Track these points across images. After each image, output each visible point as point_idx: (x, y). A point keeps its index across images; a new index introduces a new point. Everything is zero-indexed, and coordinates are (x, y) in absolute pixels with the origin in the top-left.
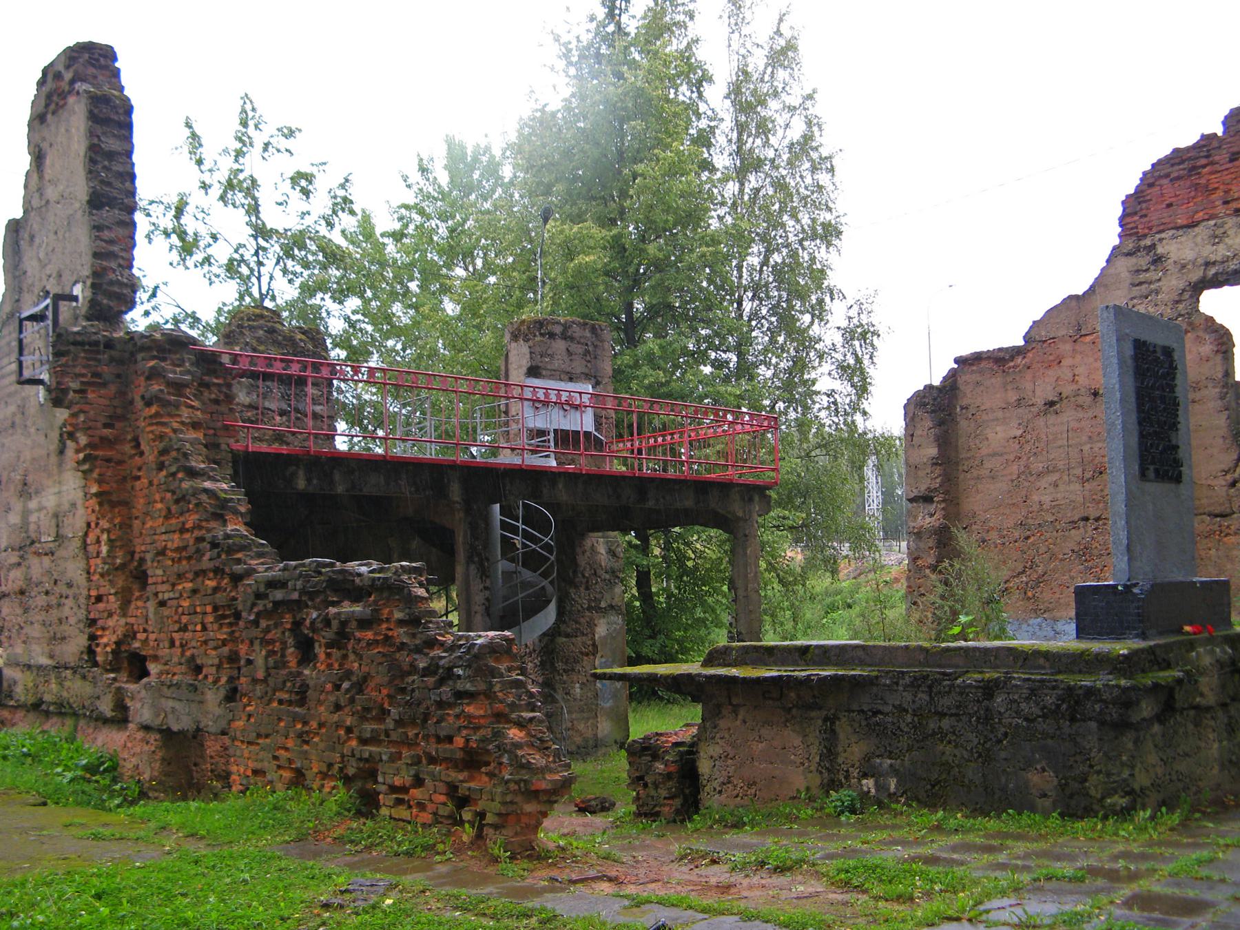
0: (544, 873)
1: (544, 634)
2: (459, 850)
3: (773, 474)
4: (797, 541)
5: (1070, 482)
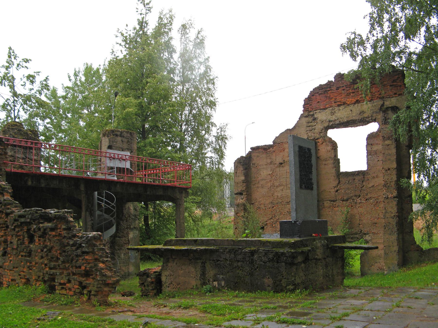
0: (110, 310)
1: (111, 237)
2: (83, 303)
3: (190, 184)
4: (199, 207)
5: (287, 189)
